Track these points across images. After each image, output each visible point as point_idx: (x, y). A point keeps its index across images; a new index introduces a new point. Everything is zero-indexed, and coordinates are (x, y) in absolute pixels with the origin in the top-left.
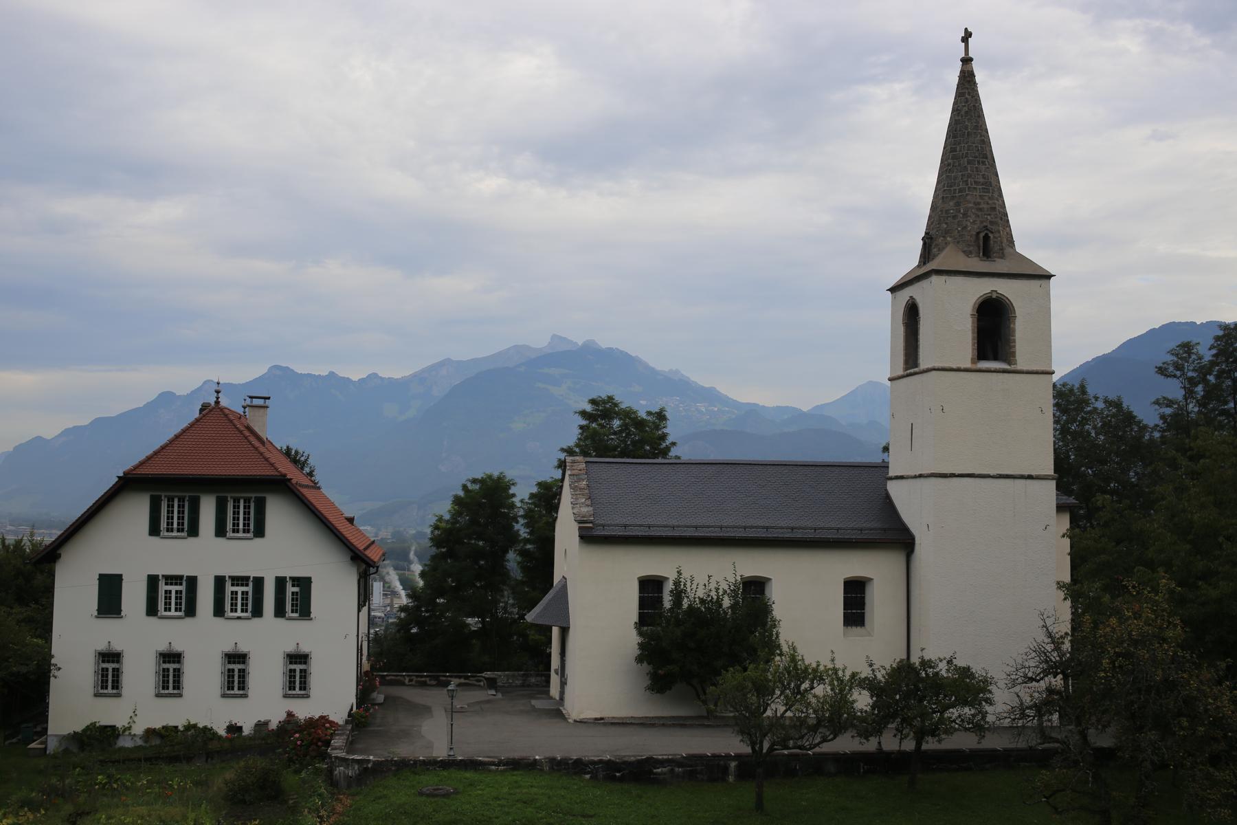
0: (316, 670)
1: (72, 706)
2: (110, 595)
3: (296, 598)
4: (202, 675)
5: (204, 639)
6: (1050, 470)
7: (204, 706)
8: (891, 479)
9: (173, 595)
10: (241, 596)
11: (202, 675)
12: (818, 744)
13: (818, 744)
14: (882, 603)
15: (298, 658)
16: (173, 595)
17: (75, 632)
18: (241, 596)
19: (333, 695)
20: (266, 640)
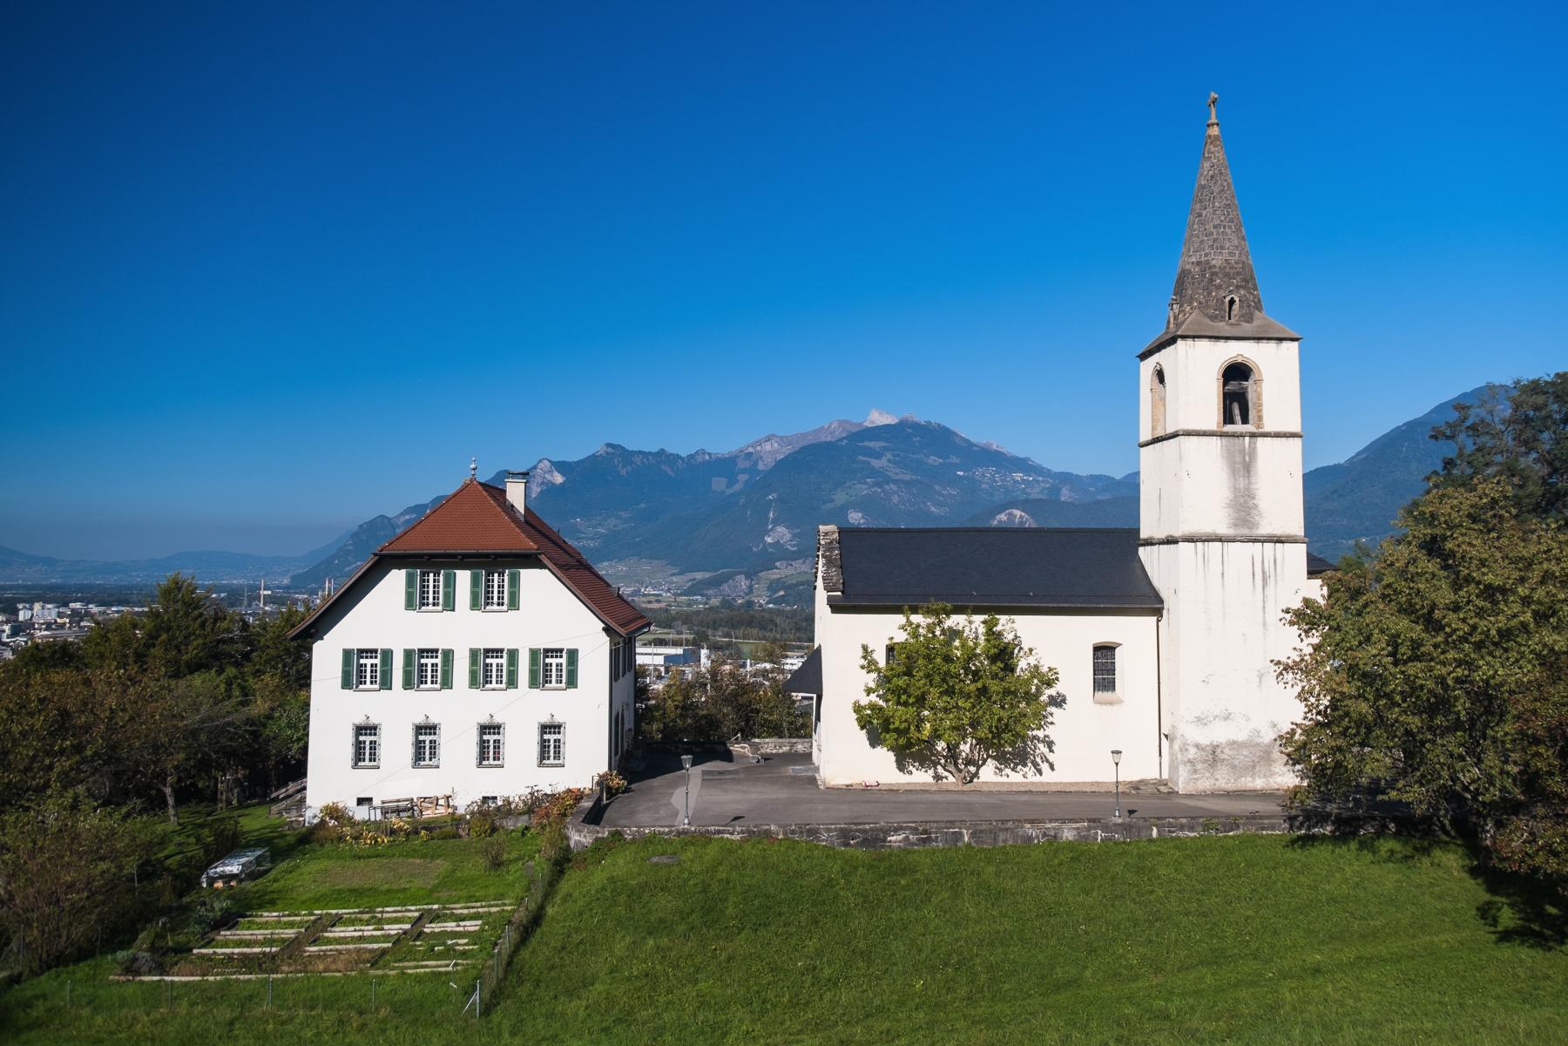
0: (444, 738)
1: (330, 782)
2: (354, 671)
3: (556, 667)
4: (458, 744)
5: (458, 710)
6: (1296, 526)
7: (459, 783)
8: (1149, 543)
9: (424, 668)
10: (489, 667)
11: (458, 744)
12: (895, 482)
13: (895, 482)
14: (1131, 667)
15: (425, 729)
16: (424, 668)
17: (331, 710)
18: (489, 667)
19: (587, 761)
20: (521, 709)
